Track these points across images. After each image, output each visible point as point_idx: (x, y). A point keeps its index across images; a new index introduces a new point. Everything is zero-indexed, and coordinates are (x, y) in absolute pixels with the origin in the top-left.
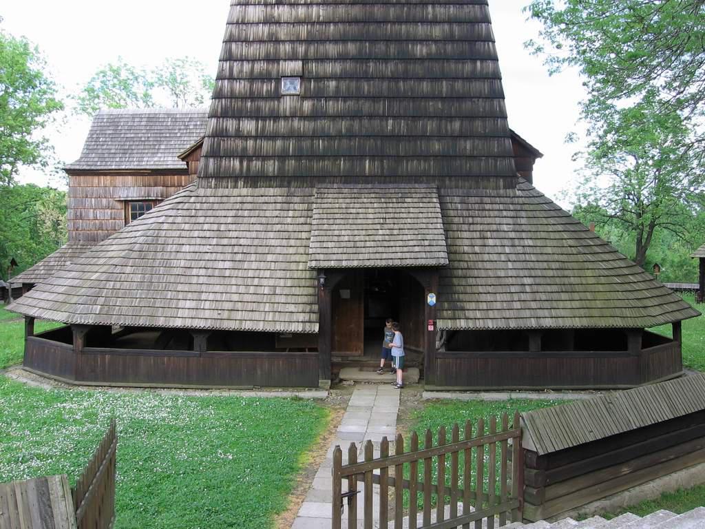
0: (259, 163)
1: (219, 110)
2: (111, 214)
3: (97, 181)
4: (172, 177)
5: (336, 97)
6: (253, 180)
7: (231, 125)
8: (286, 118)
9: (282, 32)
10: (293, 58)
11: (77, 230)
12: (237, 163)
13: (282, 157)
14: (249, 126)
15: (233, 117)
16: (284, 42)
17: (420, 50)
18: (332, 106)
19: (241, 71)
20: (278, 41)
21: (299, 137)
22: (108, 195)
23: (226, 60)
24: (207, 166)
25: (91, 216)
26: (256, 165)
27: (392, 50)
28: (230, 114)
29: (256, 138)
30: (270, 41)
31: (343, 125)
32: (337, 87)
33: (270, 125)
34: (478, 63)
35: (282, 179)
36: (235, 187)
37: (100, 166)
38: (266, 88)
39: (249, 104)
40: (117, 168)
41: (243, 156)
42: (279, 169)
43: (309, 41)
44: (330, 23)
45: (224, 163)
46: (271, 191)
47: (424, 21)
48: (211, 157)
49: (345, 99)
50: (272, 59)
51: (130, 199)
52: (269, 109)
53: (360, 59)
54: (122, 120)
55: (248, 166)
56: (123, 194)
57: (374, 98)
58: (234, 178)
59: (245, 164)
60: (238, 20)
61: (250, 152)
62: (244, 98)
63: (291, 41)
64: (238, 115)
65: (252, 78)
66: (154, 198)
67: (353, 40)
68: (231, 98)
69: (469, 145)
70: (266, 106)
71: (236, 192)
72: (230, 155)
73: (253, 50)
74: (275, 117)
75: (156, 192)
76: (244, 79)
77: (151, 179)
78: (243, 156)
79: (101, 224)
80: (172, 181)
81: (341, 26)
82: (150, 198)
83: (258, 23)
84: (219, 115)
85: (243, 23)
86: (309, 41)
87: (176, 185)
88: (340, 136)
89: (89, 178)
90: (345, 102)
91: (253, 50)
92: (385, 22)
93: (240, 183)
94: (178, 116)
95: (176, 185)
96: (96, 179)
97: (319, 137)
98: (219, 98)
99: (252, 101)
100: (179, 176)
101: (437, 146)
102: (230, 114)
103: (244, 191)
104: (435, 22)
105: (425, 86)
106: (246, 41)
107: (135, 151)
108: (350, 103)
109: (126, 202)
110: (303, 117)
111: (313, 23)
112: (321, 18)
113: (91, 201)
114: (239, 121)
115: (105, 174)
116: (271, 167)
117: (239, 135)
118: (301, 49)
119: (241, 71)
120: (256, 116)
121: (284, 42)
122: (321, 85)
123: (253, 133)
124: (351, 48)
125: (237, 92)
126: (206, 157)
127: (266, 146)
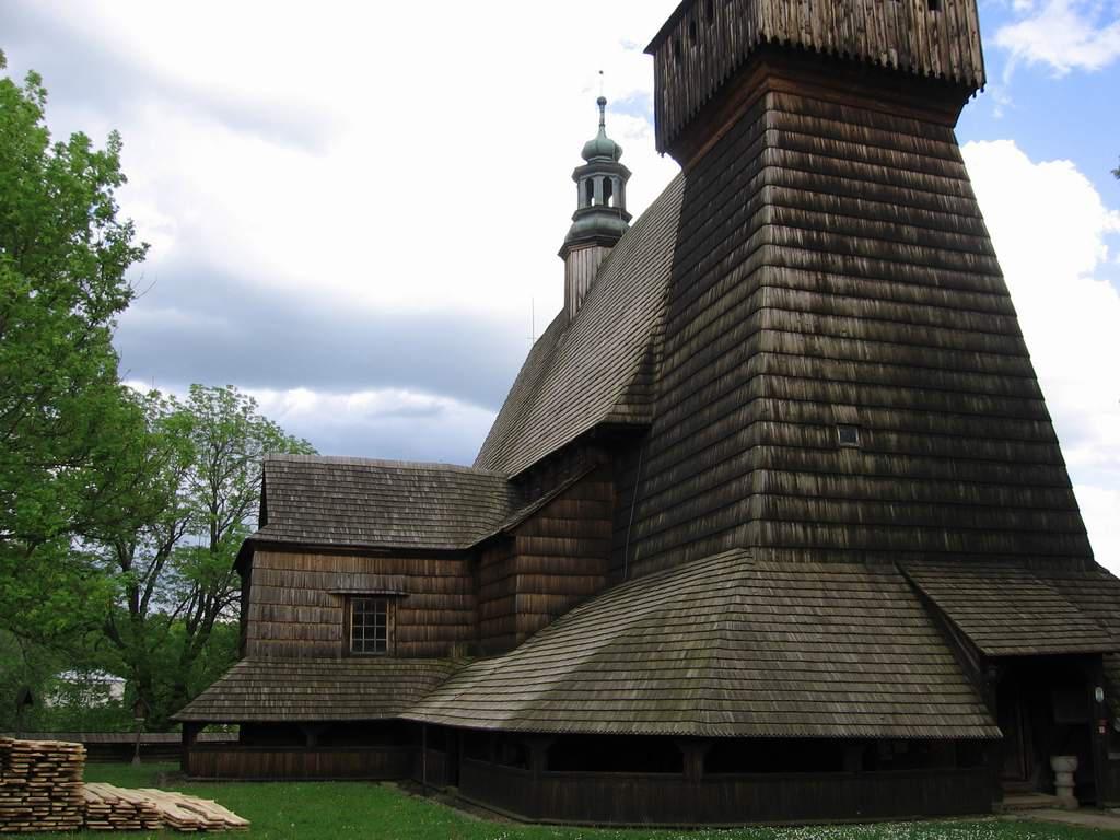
0: (826, 531)
1: (770, 460)
2: (322, 613)
3: (300, 562)
4: (421, 561)
5: (899, 454)
6: (823, 551)
7: (785, 479)
8: (848, 475)
9: (829, 369)
10: (845, 402)
11: (263, 638)
12: (800, 530)
13: (851, 523)
14: (807, 482)
15: (787, 470)
16: (831, 381)
17: (977, 404)
18: (898, 465)
19: (787, 413)
20: (824, 380)
21: (868, 500)
22: (318, 585)
23: (769, 398)
24: (763, 531)
25: (289, 617)
26: (823, 533)
27: (948, 401)
28: (783, 465)
29: (817, 498)
30: (816, 379)
31: (913, 488)
32: (899, 441)
33: (831, 483)
34: (1036, 425)
35: (855, 553)
36: (801, 561)
37: (305, 538)
38: (820, 436)
39: (803, 455)
40: (336, 542)
41: (806, 521)
42: (851, 540)
43: (859, 383)
44: (878, 363)
45: (784, 528)
46: (847, 567)
47: (975, 371)
48: (768, 520)
49: (911, 456)
50: (822, 401)
51: (355, 592)
52: (772, 458)
53: (918, 409)
54: (315, 471)
55: (813, 534)
56: (344, 585)
57: (941, 458)
58: (800, 548)
59: (809, 531)
60: (775, 349)
61: (814, 516)
62: (796, 447)
63: (840, 382)
64: (794, 469)
65: (802, 422)
66: (393, 593)
67: (908, 387)
68: (782, 446)
69: (1044, 519)
70: (823, 459)
71: (805, 567)
72: (791, 518)
73: (798, 388)
74: (834, 472)
75: (395, 583)
76: (793, 423)
77: (389, 563)
78: (806, 521)
79: (305, 631)
80: (421, 568)
81: (890, 369)
82: (387, 592)
83: (799, 355)
84: (770, 465)
85: (781, 353)
86: (859, 383)
87: (426, 573)
88: (911, 502)
89: (287, 556)
90: (911, 460)
91: (798, 388)
92: (936, 368)
93: (807, 557)
94: (426, 474)
95: (426, 573)
96: (298, 559)
97: (889, 502)
98: (766, 445)
99: (806, 452)
100: (431, 561)
101: (1013, 519)
102: (783, 465)
103: (816, 567)
104: (984, 373)
105: (989, 447)
106: (788, 375)
107: (355, 520)
108: (916, 462)
109: (347, 597)
110: (867, 476)
111: (860, 362)
112: (868, 357)
113: (289, 593)
114: (795, 475)
115: (350, 554)
116: (841, 536)
117: (797, 494)
118: (852, 392)
119: (787, 413)
120: (813, 470)
121: (831, 381)
122: (881, 436)
123: (814, 493)
124: (906, 395)
125: (787, 438)
126: (762, 519)
127: (831, 509)
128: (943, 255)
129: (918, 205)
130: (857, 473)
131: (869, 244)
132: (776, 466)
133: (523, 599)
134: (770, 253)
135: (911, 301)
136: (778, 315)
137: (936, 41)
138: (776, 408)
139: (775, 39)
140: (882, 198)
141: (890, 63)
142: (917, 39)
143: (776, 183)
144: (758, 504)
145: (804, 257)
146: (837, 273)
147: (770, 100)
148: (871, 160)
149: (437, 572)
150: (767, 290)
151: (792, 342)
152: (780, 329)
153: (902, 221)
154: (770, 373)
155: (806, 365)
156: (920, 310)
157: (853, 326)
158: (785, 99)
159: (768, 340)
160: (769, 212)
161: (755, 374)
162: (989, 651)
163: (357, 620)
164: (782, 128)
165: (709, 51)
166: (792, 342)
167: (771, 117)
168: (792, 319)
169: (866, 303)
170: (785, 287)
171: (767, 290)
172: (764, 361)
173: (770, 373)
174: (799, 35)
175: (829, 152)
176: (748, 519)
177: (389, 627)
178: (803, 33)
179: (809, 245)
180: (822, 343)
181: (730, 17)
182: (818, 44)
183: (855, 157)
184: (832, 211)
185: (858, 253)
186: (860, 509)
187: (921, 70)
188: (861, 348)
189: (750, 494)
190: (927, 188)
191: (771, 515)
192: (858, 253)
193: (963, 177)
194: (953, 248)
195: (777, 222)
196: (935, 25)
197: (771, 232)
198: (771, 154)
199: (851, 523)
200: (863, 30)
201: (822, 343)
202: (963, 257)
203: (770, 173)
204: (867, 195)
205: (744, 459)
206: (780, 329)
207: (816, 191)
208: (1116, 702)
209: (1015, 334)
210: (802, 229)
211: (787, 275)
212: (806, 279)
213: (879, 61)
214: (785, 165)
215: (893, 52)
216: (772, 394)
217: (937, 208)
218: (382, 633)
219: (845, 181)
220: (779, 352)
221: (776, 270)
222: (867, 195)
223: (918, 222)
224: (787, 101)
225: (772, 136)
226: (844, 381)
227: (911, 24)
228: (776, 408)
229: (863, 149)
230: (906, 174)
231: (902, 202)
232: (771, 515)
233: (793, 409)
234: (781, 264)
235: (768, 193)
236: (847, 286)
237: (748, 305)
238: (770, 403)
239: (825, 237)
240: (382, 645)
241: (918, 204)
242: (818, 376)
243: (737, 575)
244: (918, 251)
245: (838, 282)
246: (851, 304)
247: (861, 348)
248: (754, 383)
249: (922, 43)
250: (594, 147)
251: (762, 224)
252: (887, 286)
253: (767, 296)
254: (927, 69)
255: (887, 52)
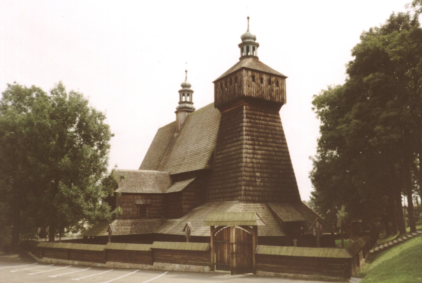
0: (254, 198)
7: (247, 188)
9: (255, 165)
10: (258, 172)
16: (255, 168)
24: (244, 198)
33: (255, 188)
38: (253, 179)
61: (252, 195)
74: (256, 186)
94: (151, 174)
110: (262, 187)
117: (250, 191)
118: (259, 170)
127: (255, 193)
128: (276, 140)
129: (272, 130)
130: (260, 186)
131: (262, 139)
132: (246, 185)
133: (184, 206)
134: (245, 142)
135: (270, 151)
136: (246, 155)
137: (277, 94)
138: (246, 174)
139: (247, 96)
140: (265, 129)
141: (268, 100)
142: (274, 94)
143: (246, 126)
144: (243, 193)
145: (250, 142)
146: (256, 145)
147: (244, 107)
148: (263, 120)
149: (158, 198)
150: (244, 150)
151: (248, 160)
152: (246, 157)
153: (268, 133)
154: (245, 167)
155: (251, 165)
156: (271, 152)
157: (259, 156)
158: (247, 107)
159: (244, 160)
160: (244, 133)
161: (241, 167)
162: (284, 221)
163: (140, 210)
164: (247, 114)
165: (230, 91)
166: (248, 160)
167: (245, 111)
168: (248, 155)
169: (262, 152)
170: (247, 149)
171: (244, 150)
172: (244, 164)
173: (245, 167)
174: (251, 94)
175: (256, 119)
176: (241, 195)
177: (147, 212)
178: (252, 94)
179: (252, 140)
180: (254, 160)
181: (236, 87)
182: (255, 96)
183: (260, 119)
184: (256, 132)
185: (261, 141)
186: (260, 193)
187: (274, 101)
188: (261, 161)
189: (241, 190)
190: (274, 126)
191: (245, 195)
192: (261, 141)
193: (280, 123)
194: (278, 139)
195: (246, 135)
196: (277, 90)
197: (245, 137)
198: (245, 120)
199: (259, 196)
200: (263, 92)
201: (254, 160)
202: (280, 141)
203: (245, 124)
204: (262, 128)
205: (239, 183)
206: (246, 157)
207: (253, 128)
208: (2, 115)
209: (288, 156)
210: (250, 136)
211: (248, 146)
212: (251, 147)
213: (266, 99)
214: (247, 122)
215: (269, 97)
216: (245, 171)
217: (275, 130)
218: (146, 213)
219: (258, 125)
220: (246, 162)
221: (245, 145)
222: (262, 128)
223: (271, 134)
224: (248, 107)
225: (245, 116)
226: (258, 168)
227: (273, 90)
228: (246, 174)
229: (262, 118)
230: (270, 123)
231: (268, 129)
232: (245, 195)
233: (249, 174)
234: (246, 144)
235: (244, 128)
236: (258, 148)
237: (239, 151)
238: (244, 173)
239: (255, 138)
240: (146, 216)
241: (272, 130)
242: (253, 167)
243: (240, 206)
244: (271, 140)
245: (257, 147)
246: (259, 152)
247: (261, 161)
248: (241, 169)
249: (275, 94)
250: (185, 85)
251: (242, 135)
252: (266, 148)
253: (244, 151)
254: (275, 101)
255: (268, 97)
